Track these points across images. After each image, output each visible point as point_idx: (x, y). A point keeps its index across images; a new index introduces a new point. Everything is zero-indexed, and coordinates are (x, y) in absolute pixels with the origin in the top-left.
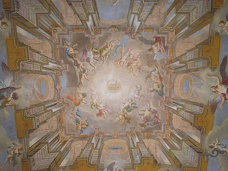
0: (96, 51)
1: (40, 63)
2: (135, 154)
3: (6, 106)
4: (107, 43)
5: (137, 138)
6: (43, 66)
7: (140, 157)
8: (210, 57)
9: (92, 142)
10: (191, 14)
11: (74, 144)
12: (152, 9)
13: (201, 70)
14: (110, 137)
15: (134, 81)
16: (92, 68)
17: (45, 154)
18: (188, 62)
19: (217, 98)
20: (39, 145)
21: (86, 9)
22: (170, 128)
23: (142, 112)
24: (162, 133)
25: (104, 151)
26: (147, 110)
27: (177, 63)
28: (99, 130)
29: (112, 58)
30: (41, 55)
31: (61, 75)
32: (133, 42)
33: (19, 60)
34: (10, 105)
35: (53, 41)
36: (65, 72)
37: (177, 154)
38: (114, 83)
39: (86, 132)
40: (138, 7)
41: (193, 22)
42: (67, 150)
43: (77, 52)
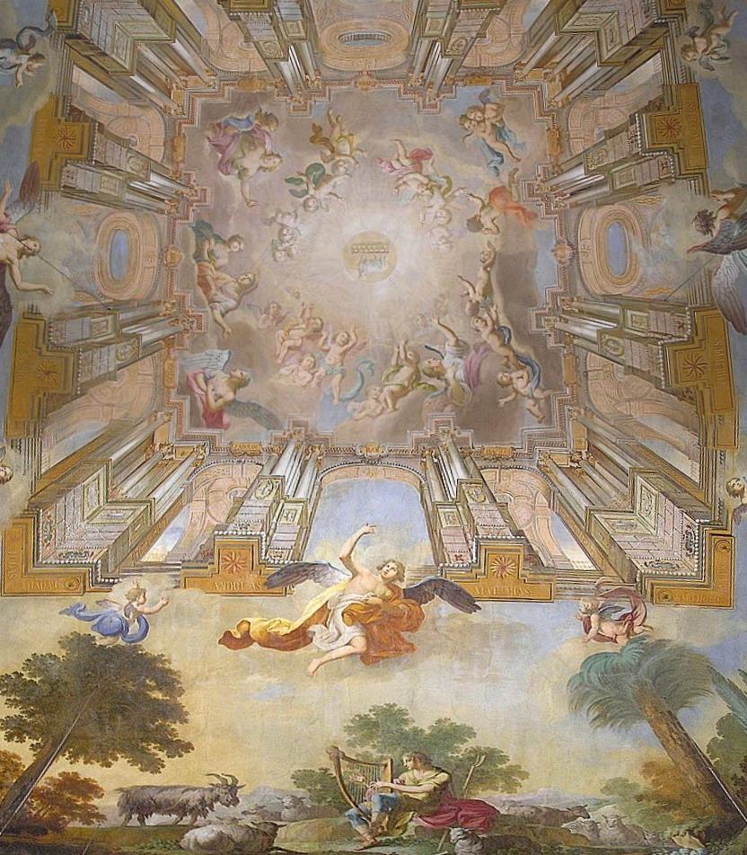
0: (434, 382)
1: (628, 334)
2: (293, 21)
3: (735, 191)
4: (396, 410)
5: (287, 73)
6: (615, 325)
7: (276, 9)
8: (40, 354)
9: (446, 61)
10: (101, 501)
11: (512, 56)
12: (233, 513)
13: (70, 310)
14: (382, 77)
15: (298, 276)
16: (446, 320)
17: (608, 27)
18: (113, 339)
19: (21, 216)
20: (630, 58)
21: (463, 519)
22: (172, 112)
23: (270, 164)
24: (202, 95)
25: (405, 30)
26: (251, 173)
27: (148, 335)
28: (424, 101)
29: (376, 358)
30: (621, 362)
31: (554, 295)
32: (302, 412)
33: (693, 343)
34: (722, 193)
35: (583, 412)
36: (541, 306)
37: (148, 27)
38: (371, 269)
39: (467, 94)
40: (283, 520)
41: (95, 475)
42: (534, 37)
43: (500, 375)
